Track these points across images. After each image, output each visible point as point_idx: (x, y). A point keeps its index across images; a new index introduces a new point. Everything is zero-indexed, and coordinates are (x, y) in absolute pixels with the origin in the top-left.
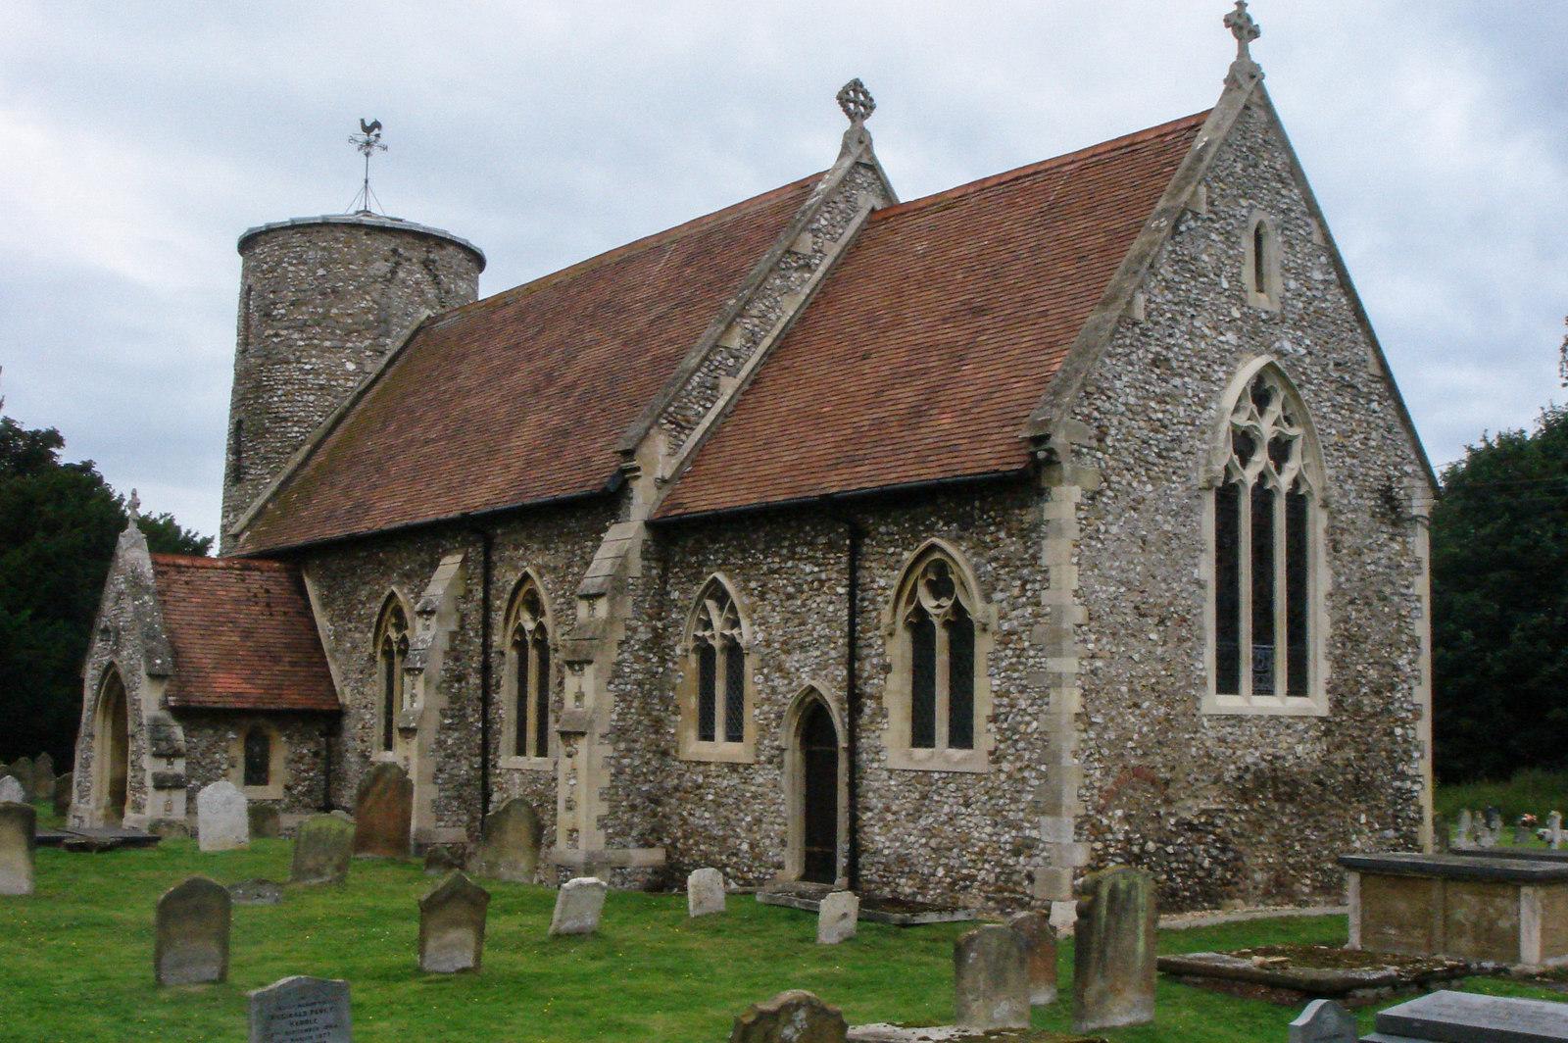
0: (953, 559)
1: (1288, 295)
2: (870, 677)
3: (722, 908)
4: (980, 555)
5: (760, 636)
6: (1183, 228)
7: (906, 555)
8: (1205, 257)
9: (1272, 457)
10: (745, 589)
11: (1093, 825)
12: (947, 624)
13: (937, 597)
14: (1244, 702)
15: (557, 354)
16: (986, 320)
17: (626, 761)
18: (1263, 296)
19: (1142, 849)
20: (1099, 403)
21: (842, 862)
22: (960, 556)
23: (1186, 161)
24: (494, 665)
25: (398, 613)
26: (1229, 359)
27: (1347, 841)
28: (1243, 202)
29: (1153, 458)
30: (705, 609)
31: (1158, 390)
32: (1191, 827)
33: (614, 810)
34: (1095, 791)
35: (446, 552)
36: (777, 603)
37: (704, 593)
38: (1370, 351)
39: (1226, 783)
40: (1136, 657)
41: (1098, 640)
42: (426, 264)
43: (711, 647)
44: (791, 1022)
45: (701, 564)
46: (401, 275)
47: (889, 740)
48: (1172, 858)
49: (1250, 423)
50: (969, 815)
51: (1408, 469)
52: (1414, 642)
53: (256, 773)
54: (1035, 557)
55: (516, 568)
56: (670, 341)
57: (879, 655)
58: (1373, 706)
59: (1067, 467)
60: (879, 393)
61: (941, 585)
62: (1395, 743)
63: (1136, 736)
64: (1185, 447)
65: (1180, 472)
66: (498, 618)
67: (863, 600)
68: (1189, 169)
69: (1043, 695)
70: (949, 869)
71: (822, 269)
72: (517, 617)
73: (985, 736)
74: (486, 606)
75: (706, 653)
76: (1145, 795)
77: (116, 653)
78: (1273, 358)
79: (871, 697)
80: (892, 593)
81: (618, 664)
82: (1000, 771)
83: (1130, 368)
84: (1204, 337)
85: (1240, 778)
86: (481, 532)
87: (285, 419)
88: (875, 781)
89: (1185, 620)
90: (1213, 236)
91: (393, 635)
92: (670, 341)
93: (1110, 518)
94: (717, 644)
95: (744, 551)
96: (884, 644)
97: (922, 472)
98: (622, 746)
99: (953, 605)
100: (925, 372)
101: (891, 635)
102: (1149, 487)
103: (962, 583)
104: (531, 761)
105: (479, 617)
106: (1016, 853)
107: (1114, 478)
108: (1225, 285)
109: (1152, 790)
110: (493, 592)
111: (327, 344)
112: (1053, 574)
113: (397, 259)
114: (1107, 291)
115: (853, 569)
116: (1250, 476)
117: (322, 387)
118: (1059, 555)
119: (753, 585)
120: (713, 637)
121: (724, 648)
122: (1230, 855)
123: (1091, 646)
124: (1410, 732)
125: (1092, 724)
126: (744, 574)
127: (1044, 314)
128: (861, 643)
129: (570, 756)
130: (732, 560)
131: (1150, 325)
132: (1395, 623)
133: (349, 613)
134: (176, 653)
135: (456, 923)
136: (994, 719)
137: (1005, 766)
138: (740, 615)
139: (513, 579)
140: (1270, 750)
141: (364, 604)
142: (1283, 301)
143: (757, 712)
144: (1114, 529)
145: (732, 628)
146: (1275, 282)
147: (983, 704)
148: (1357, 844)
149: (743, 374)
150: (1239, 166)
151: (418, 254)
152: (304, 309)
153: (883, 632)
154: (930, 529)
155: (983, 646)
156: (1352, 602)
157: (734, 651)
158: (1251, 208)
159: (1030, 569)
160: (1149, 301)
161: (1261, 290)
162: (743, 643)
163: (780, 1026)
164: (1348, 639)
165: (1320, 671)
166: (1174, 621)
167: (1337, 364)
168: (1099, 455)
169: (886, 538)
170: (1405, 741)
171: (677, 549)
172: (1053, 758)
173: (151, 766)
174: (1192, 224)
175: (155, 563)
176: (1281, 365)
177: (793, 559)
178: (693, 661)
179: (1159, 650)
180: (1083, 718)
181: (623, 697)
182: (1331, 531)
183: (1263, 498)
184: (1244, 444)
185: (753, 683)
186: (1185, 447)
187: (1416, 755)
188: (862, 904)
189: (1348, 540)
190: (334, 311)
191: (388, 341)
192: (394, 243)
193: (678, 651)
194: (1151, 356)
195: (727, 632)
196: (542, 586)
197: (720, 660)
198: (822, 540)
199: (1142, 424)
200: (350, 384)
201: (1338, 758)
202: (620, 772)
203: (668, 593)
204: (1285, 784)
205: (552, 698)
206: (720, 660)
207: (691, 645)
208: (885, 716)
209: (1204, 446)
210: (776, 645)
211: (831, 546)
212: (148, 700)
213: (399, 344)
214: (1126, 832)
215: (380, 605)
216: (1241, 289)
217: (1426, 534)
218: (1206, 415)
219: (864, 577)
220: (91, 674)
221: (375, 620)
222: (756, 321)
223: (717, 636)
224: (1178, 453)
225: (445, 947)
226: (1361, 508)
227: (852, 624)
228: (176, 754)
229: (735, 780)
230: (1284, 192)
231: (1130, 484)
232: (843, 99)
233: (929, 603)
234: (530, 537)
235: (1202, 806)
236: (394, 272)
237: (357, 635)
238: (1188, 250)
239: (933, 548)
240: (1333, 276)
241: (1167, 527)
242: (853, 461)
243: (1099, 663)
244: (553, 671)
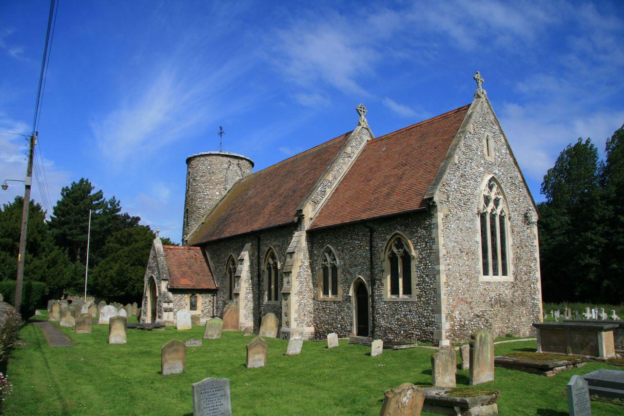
0: (403, 237)
1: (496, 157)
2: (378, 274)
3: (338, 345)
4: (412, 235)
5: (342, 263)
6: (467, 136)
7: (388, 236)
8: (473, 145)
9: (495, 205)
10: (337, 249)
11: (451, 316)
12: (402, 257)
13: (398, 249)
14: (490, 278)
15: (276, 186)
16: (406, 167)
17: (303, 301)
18: (489, 157)
20: (446, 188)
21: (370, 330)
23: (466, 118)
24: (261, 274)
25: (233, 261)
26: (481, 175)
27: (520, 319)
28: (483, 129)
29: (462, 205)
31: (463, 184)
32: (478, 316)
33: (299, 316)
34: (451, 306)
35: (246, 243)
36: (347, 253)
37: (324, 251)
38: (519, 173)
39: (487, 302)
40: (461, 265)
41: (450, 260)
42: (238, 165)
43: (327, 267)
44: (405, 395)
45: (323, 243)
46: (231, 168)
48: (473, 326)
49: (488, 194)
50: (411, 314)
51: (531, 208)
52: (535, 259)
53: (193, 307)
54: (430, 235)
55: (267, 246)
56: (311, 180)
57: (380, 267)
58: (525, 278)
59: (439, 207)
60: (375, 190)
62: (531, 289)
63: (461, 289)
64: (471, 201)
65: (470, 209)
66: (262, 261)
67: (374, 251)
68: (465, 122)
69: (434, 277)
70: (405, 331)
71: (354, 157)
72: (268, 260)
73: (415, 290)
74: (259, 257)
75: (325, 269)
76: (465, 307)
78: (493, 175)
81: (299, 272)
82: (421, 301)
83: (455, 178)
84: (474, 169)
85: (490, 300)
86: (256, 237)
87: (200, 208)
88: (381, 306)
89: (473, 253)
90: (475, 139)
91: (231, 267)
92: (311, 180)
93: (451, 222)
94: (329, 266)
95: (336, 238)
96: (382, 264)
97: (392, 211)
98: (301, 297)
99: (403, 251)
100: (389, 183)
101: (384, 261)
102: (462, 213)
103: (407, 245)
105: (257, 261)
106: (427, 326)
107: (452, 210)
108: (479, 154)
109: (466, 305)
110: (261, 254)
111: (211, 187)
113: (230, 164)
114: (447, 155)
115: (371, 241)
116: (489, 210)
117: (210, 199)
119: (339, 248)
120: (327, 264)
122: (489, 324)
123: (448, 261)
124: (536, 286)
125: (449, 285)
126: (336, 245)
127: (426, 164)
128: (374, 264)
129: (285, 300)
130: (333, 241)
131: (460, 165)
132: (529, 254)
133: (219, 261)
134: (170, 274)
135: (258, 353)
136: (418, 285)
137: (422, 299)
138: (336, 257)
139: (267, 249)
140: (498, 292)
141: (223, 258)
142: (495, 159)
143: (342, 285)
144: (453, 226)
145: (325, 262)
146: (492, 153)
147: (414, 281)
148: (523, 320)
149: (333, 187)
150: (481, 119)
151: (236, 161)
152: (204, 178)
154: (395, 228)
156: (518, 247)
157: (334, 268)
160: (459, 158)
161: (489, 156)
162: (337, 265)
163: (402, 398)
164: (518, 259)
165: (511, 268)
166: (470, 253)
167: (510, 177)
168: (448, 203)
169: (381, 232)
170: (534, 288)
171: (316, 239)
174: (469, 135)
175: (164, 248)
176: (496, 177)
177: (352, 239)
178: (321, 271)
179: (467, 262)
182: (512, 227)
183: (493, 217)
184: (487, 200)
186: (471, 201)
187: (537, 293)
188: (384, 343)
190: (213, 178)
191: (228, 186)
192: (229, 159)
193: (317, 268)
194: (460, 174)
195: (323, 263)
197: (330, 271)
198: (342, 233)
199: (459, 194)
200: (217, 198)
201: (516, 294)
203: (313, 252)
204: (503, 302)
205: (279, 283)
206: (330, 271)
207: (321, 266)
208: (383, 285)
209: (477, 201)
210: (347, 265)
211: (364, 235)
213: (231, 187)
214: (460, 318)
215: (227, 258)
216: (484, 155)
217: (537, 227)
218: (476, 192)
219: (374, 244)
220: (146, 280)
221: (226, 263)
222: (336, 172)
223: (329, 263)
224: (469, 203)
225: (255, 360)
226: (519, 220)
227: (371, 258)
228: (171, 302)
230: (493, 127)
231: (456, 212)
233: (395, 250)
234: (271, 237)
235: (481, 310)
236: (229, 167)
237: (221, 267)
238: (469, 143)
239: (397, 234)
240: (508, 152)
241: (467, 225)
242: (371, 209)
243: (450, 267)
244: (279, 275)
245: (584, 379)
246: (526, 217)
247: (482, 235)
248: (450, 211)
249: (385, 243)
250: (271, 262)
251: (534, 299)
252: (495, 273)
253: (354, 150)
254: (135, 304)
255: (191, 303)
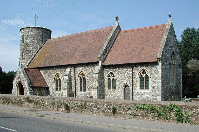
7: (139, 70)
30: (109, 75)
42: (46, 33)
55: (80, 70)
61: (144, 72)
72: (80, 76)
77: (20, 80)
79: (135, 84)
80: (138, 74)
86: (74, 66)
94: (111, 79)
104: (83, 92)
121: (112, 80)
153: (136, 77)
181: (100, 85)
185: (117, 83)
189: (177, 69)
196: (85, 73)
205: (87, 85)
212: (26, 84)
229: (115, 93)
232: (118, 19)
233: (142, 75)
239: (143, 69)
251: (180, 92)
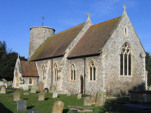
17: (64, 81)
19: (112, 90)
22: (94, 63)
46: (46, 32)
47: (88, 79)
52: (143, 70)
53: (30, 82)
61: (93, 65)
66: (53, 67)
73: (96, 79)
94: (73, 70)
112: (102, 63)
116: (124, 53)
118: (103, 61)
139: (55, 63)
155: (96, 70)
158: (125, 26)
159: (100, 64)
172: (102, 81)
173: (20, 82)
180: (105, 78)
185: (76, 73)
196: (57, 64)
202: (64, 82)
206: (73, 72)
212: (20, 75)
220: (14, 73)
236: (45, 32)
239: (92, 60)
245: (49, 98)
246: (141, 56)
247: (121, 62)
248: (108, 54)
249: (89, 63)
250: (56, 68)
252: (126, 74)
253: (85, 30)
254: (12, 81)
255: (30, 81)
